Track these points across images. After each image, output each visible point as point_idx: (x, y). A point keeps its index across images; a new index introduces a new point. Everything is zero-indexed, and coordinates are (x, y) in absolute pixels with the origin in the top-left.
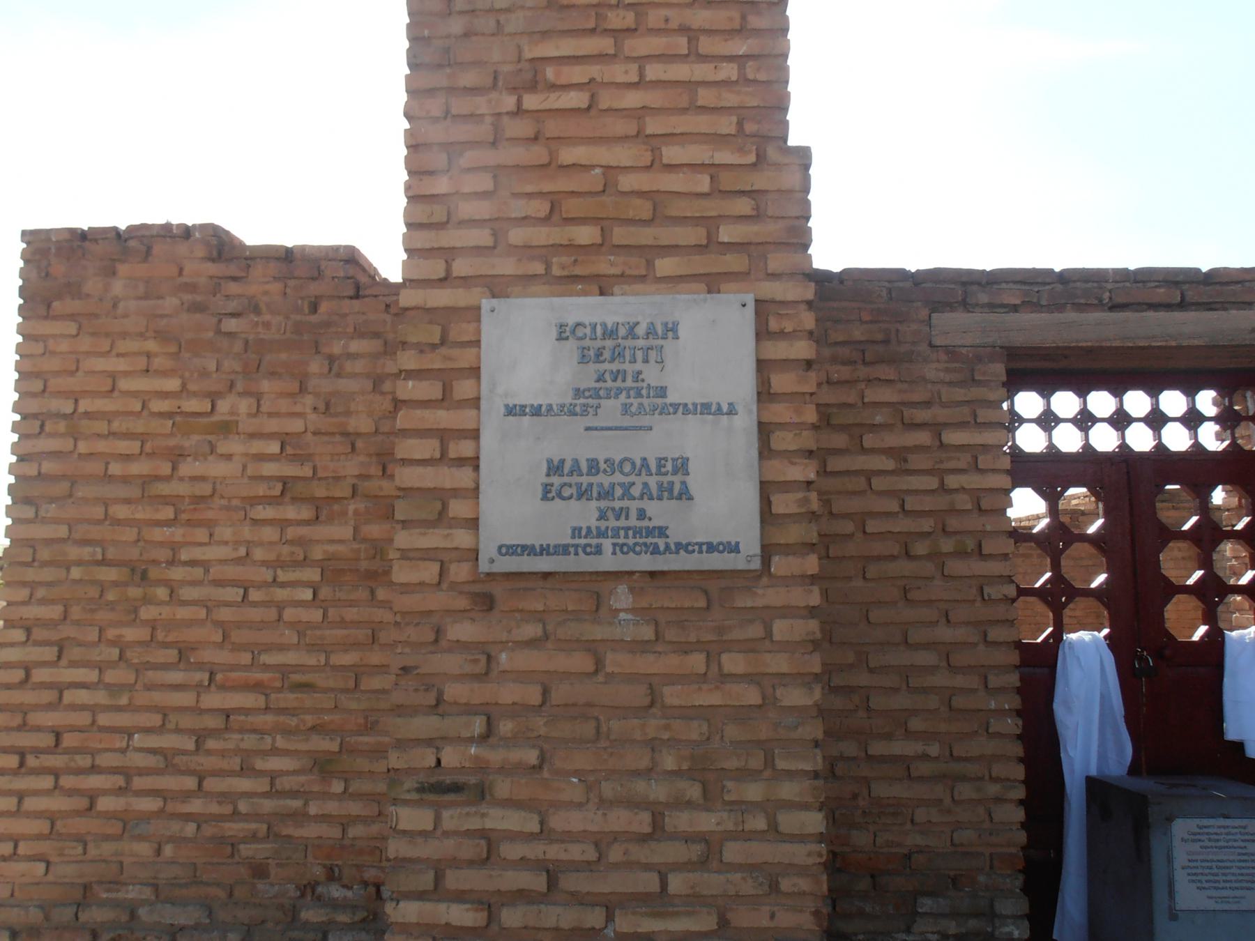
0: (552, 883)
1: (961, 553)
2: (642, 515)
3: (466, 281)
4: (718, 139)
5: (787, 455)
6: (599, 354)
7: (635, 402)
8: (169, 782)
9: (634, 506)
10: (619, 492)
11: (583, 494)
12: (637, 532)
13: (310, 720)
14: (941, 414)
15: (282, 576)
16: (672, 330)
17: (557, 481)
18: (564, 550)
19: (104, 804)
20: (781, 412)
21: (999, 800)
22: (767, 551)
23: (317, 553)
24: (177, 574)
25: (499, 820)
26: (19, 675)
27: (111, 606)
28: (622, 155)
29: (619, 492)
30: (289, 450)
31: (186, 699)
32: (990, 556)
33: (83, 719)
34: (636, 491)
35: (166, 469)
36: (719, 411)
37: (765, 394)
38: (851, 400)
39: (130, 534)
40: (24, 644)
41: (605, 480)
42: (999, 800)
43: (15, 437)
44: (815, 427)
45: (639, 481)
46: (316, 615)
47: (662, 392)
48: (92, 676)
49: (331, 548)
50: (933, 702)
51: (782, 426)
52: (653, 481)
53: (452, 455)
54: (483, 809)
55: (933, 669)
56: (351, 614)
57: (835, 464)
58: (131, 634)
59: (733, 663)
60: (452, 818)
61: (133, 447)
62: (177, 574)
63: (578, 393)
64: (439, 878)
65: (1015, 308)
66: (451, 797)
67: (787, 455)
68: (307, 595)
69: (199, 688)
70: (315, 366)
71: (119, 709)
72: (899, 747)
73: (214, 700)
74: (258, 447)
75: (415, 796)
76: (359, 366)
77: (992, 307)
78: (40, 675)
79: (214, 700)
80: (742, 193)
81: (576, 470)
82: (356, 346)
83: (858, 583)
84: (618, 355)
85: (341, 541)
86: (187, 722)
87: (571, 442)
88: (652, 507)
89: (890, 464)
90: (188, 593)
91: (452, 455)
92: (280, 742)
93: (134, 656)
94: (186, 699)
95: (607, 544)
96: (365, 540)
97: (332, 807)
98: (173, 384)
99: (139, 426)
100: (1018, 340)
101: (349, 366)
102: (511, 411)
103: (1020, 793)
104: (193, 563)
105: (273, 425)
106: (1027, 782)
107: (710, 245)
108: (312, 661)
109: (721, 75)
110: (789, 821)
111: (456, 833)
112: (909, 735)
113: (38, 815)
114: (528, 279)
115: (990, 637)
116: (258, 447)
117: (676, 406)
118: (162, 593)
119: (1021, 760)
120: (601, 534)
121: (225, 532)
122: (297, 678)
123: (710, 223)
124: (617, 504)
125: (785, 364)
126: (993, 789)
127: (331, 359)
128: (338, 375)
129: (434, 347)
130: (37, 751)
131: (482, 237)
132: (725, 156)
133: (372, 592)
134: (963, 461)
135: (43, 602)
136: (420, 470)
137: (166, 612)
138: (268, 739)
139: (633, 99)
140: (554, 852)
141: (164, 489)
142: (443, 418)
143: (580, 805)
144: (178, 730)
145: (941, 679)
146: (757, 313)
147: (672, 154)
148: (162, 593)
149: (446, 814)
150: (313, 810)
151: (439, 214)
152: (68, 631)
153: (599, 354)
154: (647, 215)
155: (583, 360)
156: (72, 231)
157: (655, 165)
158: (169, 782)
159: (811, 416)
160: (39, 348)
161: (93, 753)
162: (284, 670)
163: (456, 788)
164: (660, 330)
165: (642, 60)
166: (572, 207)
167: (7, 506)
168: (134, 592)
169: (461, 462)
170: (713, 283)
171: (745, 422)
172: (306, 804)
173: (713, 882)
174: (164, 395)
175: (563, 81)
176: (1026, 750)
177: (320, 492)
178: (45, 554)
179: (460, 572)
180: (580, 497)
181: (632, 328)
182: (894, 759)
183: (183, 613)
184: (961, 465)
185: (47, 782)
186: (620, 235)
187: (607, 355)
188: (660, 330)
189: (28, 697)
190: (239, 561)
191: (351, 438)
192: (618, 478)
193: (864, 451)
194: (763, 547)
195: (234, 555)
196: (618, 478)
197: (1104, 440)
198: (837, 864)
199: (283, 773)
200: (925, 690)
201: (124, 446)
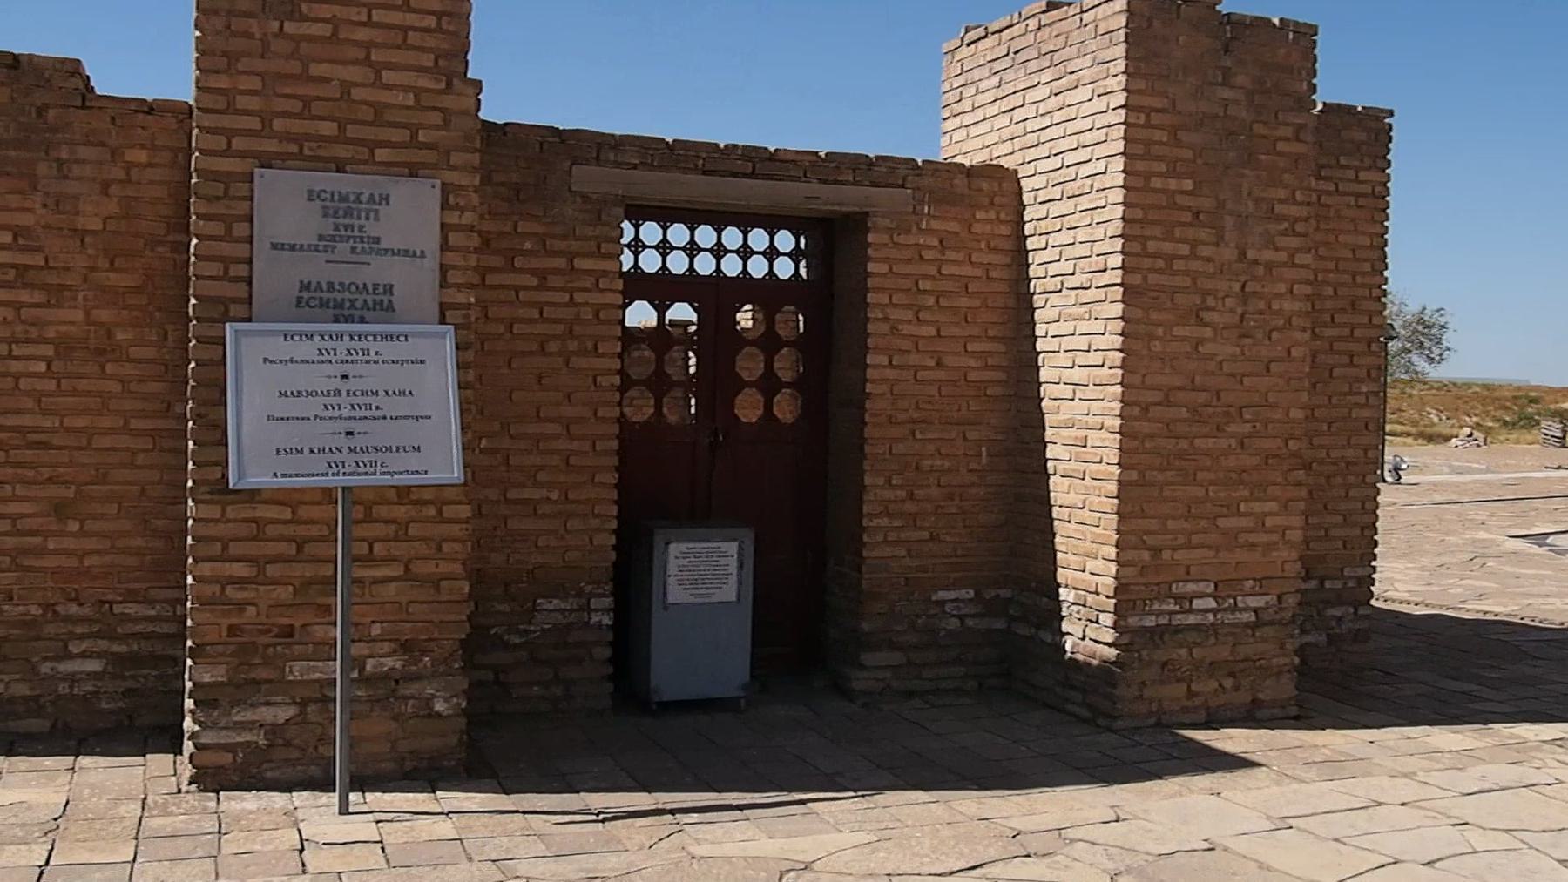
0: (299, 549)
1: (583, 352)
3: (243, 155)
4: (421, 70)
5: (459, 286)
6: (336, 212)
7: (359, 246)
10: (348, 304)
13: (46, 472)
14: (575, 246)
16: (385, 199)
17: (305, 295)
20: (453, 258)
21: (598, 530)
29: (348, 304)
30: (21, 241)
32: (603, 355)
34: (358, 304)
36: (414, 255)
37: (445, 247)
38: (507, 229)
41: (339, 297)
42: (598, 530)
44: (476, 250)
45: (361, 298)
46: (51, 385)
47: (377, 240)
49: (63, 328)
50: (556, 460)
51: (455, 267)
52: (370, 299)
53: (232, 274)
55: (557, 436)
56: (83, 384)
57: (492, 279)
63: (321, 238)
64: (225, 548)
65: (635, 167)
67: (459, 286)
68: (42, 367)
70: (42, 169)
72: (527, 494)
75: (208, 497)
76: (88, 171)
77: (618, 164)
80: (435, 109)
81: (319, 287)
82: (83, 152)
83: (505, 370)
84: (348, 213)
85: (72, 323)
89: (534, 282)
91: (232, 274)
92: (20, 490)
96: (94, 324)
97: (69, 543)
101: (76, 170)
102: (274, 246)
103: (614, 525)
107: (414, 143)
109: (424, 24)
111: (235, 521)
112: (537, 485)
115: (600, 414)
117: (386, 250)
119: (616, 502)
123: (414, 130)
124: (346, 312)
125: (458, 228)
126: (595, 522)
127: (60, 162)
128: (66, 177)
129: (218, 198)
131: (254, 123)
132: (424, 82)
133: (103, 368)
134: (588, 282)
139: (362, 34)
140: (301, 530)
143: (319, 503)
145: (562, 445)
146: (443, 191)
149: (229, 509)
150: (51, 545)
151: (221, 103)
153: (336, 212)
154: (370, 118)
155: (325, 215)
159: (476, 241)
162: (21, 430)
164: (377, 199)
166: (317, 108)
169: (237, 279)
170: (413, 171)
171: (431, 263)
173: (399, 549)
176: (620, 494)
177: (53, 279)
180: (322, 306)
181: (358, 196)
182: (525, 502)
184: (588, 285)
187: (341, 213)
188: (377, 199)
191: (81, 234)
192: (347, 295)
193: (514, 269)
196: (347, 295)
197: (705, 265)
198: (478, 576)
199: (22, 516)
200: (552, 452)
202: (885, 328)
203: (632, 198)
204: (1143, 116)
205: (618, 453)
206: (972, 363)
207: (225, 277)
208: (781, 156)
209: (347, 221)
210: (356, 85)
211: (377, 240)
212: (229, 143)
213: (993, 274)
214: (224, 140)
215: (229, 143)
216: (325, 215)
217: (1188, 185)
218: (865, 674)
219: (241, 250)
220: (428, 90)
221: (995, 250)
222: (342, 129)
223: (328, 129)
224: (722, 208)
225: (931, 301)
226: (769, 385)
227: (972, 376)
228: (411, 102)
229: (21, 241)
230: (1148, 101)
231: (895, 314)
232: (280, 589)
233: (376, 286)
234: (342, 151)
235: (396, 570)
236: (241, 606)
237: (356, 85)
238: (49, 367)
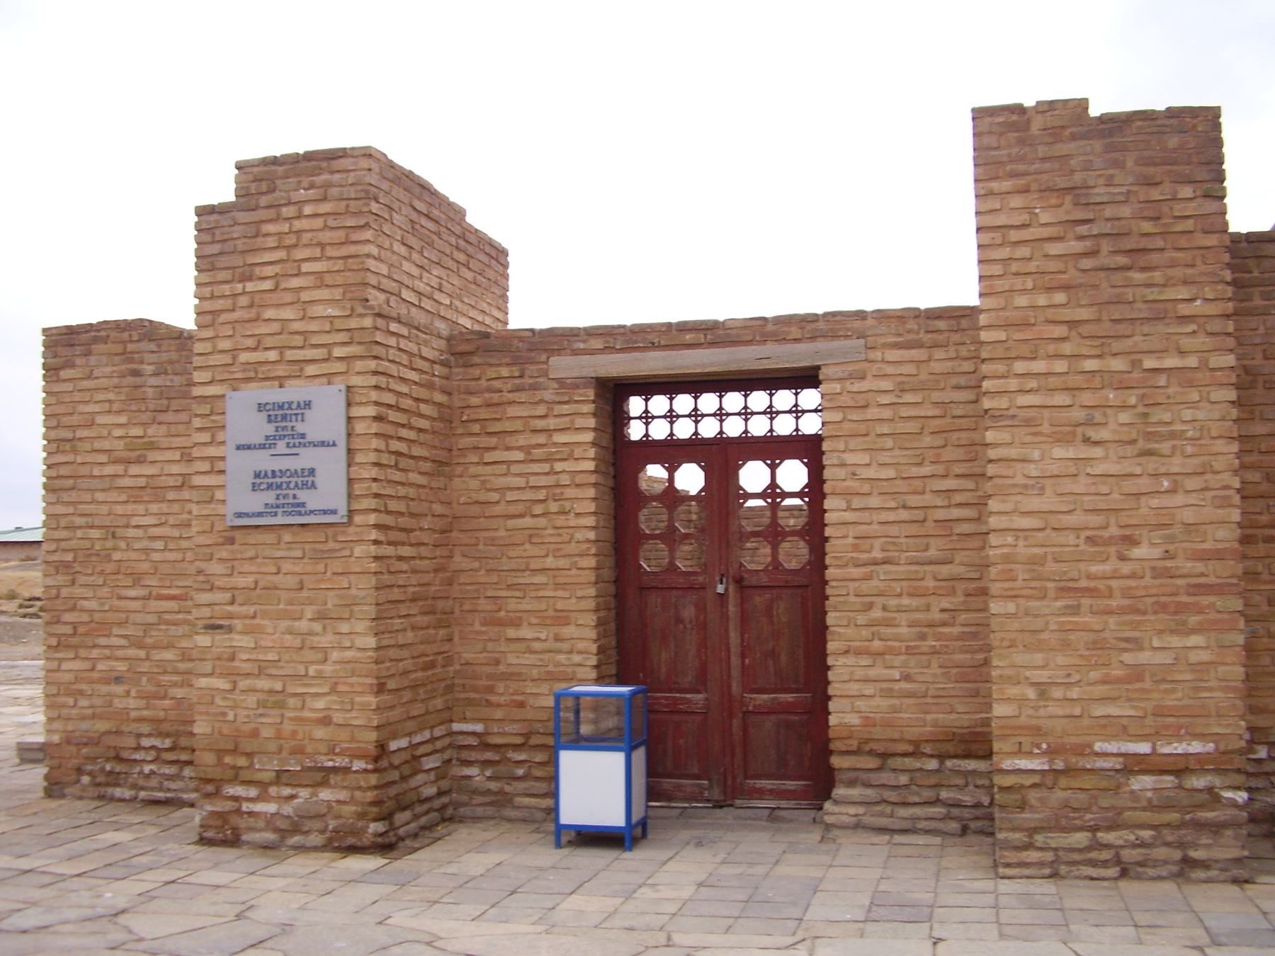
2: (295, 497)
8: (132, 652)
9: (291, 492)
10: (284, 486)
11: (270, 486)
12: (293, 505)
17: (258, 481)
18: (260, 514)
22: (351, 513)
24: (131, 533)
28: (287, 313)
34: (292, 485)
39: (104, 509)
41: (278, 480)
43: (45, 454)
45: (293, 480)
54: (232, 636)
62: (131, 533)
63: (267, 438)
84: (284, 418)
87: (263, 460)
88: (299, 493)
98: (123, 419)
100: (602, 373)
104: (137, 527)
114: (248, 380)
136: (202, 477)
137: (126, 556)
142: (212, 451)
148: (123, 545)
154: (300, 344)
155: (270, 421)
156: (68, 327)
160: (53, 400)
167: (1083, 104)
170: (329, 377)
172: (351, 762)
175: (264, 275)
178: (63, 523)
179: (218, 527)
186: (290, 355)
194: (350, 511)
196: (285, 479)
197: (709, 429)
202: (841, 473)
204: (256, 301)
208: (729, 325)
209: (284, 424)
211: (303, 436)
216: (270, 421)
224: (755, 376)
230: (1001, 220)
231: (850, 458)
234: (281, 371)
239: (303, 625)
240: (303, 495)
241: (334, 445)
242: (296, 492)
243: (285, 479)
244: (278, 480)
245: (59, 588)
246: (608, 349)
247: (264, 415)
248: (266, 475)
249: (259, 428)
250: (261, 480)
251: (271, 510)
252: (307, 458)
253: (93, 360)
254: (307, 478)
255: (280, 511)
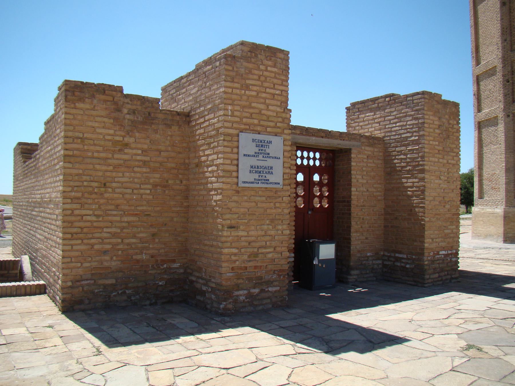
2: (265, 177)
8: (114, 241)
9: (264, 175)
11: (256, 172)
12: (265, 180)
15: (142, 187)
16: (271, 142)
17: (252, 169)
18: (252, 183)
19: (96, 247)
23: (151, 181)
24: (114, 185)
25: (241, 233)
26: (70, 212)
27: (96, 193)
30: (144, 153)
31: (118, 218)
33: (88, 224)
34: (264, 172)
35: (110, 156)
39: (100, 174)
40: (71, 203)
41: (259, 170)
46: (151, 197)
47: (269, 154)
48: (91, 212)
58: (102, 201)
59: (278, 205)
60: (233, 234)
61: (101, 149)
62: (114, 185)
63: (255, 153)
66: (233, 229)
68: (148, 192)
69: (121, 216)
71: (100, 221)
73: (125, 219)
74: (135, 151)
78: (77, 212)
79: (125, 219)
84: (262, 146)
86: (118, 225)
87: (254, 162)
90: (118, 190)
93: (103, 207)
94: (118, 218)
95: (260, 182)
99: (102, 143)
102: (244, 155)
104: (118, 182)
105: (139, 146)
106: (295, 235)
108: (150, 209)
110: (284, 232)
113: (77, 251)
116: (135, 151)
118: (110, 190)
120: (259, 180)
121: (127, 174)
122: (146, 213)
124: (262, 175)
130: (76, 234)
132: (279, 109)
135: (77, 192)
138: (139, 229)
139: (264, 95)
141: (110, 161)
144: (116, 227)
147: (271, 108)
150: (151, 246)
152: (84, 200)
155: (257, 146)
157: (268, 109)
158: (114, 241)
161: (92, 233)
163: (234, 227)
165: (266, 88)
168: (103, 189)
169: (234, 165)
174: (109, 135)
181: (264, 141)
183: (116, 195)
185: (79, 242)
189: (73, 218)
190: (130, 182)
195: (129, 180)
196: (262, 170)
201: (98, 148)
203: (300, 144)
205: (295, 216)
206: (375, 190)
207: (231, 164)
209: (262, 148)
210: (263, 110)
211: (269, 154)
212: (232, 125)
213: (379, 166)
214: (231, 124)
215: (232, 125)
216: (257, 146)
217: (437, 143)
218: (351, 277)
219: (235, 156)
220: (279, 112)
221: (378, 159)
222: (259, 122)
223: (256, 122)
225: (365, 173)
226: (321, 197)
227: (375, 194)
228: (275, 115)
229: (144, 153)
231: (358, 177)
232: (244, 256)
233: (258, 166)
234: (259, 128)
235: (272, 250)
236: (235, 261)
237: (263, 110)
238: (151, 191)
239: (265, 227)
240: (268, 177)
241: (279, 158)
242: (266, 175)
243: (262, 170)
244: (259, 170)
245: (73, 210)
246: (301, 134)
247: (254, 144)
248: (255, 167)
249: (252, 149)
250: (254, 169)
251: (257, 181)
252: (270, 162)
253: (95, 101)
254: (270, 170)
255: (260, 182)
